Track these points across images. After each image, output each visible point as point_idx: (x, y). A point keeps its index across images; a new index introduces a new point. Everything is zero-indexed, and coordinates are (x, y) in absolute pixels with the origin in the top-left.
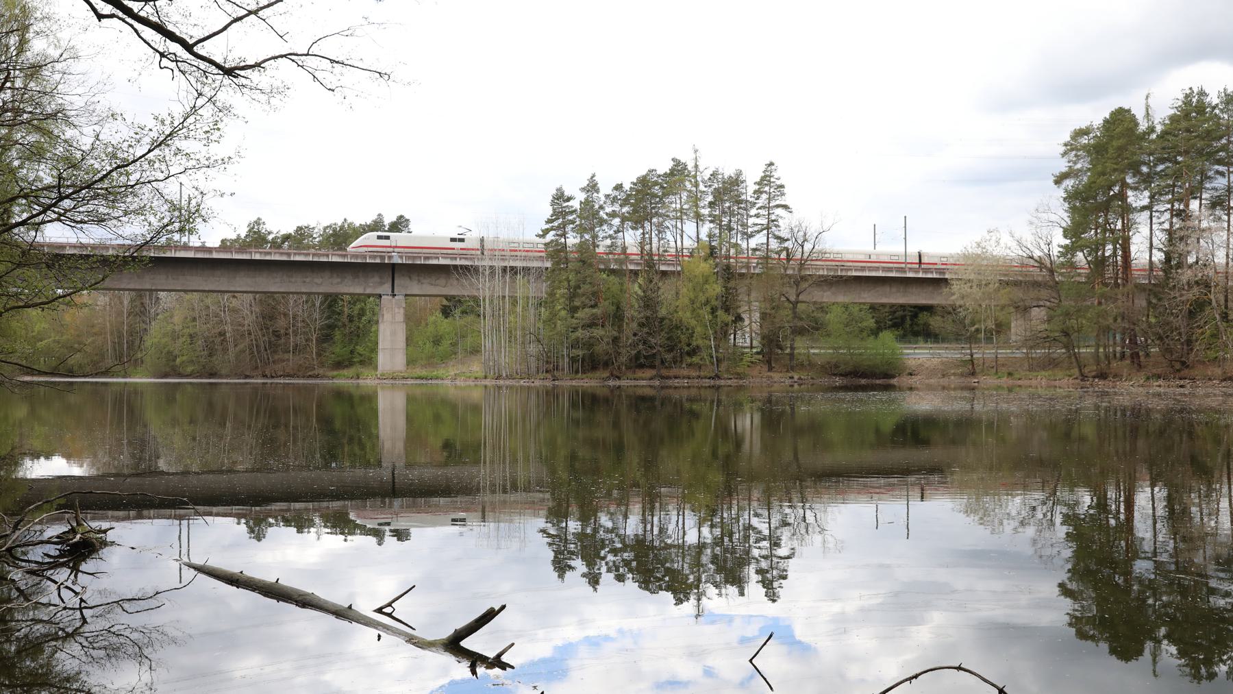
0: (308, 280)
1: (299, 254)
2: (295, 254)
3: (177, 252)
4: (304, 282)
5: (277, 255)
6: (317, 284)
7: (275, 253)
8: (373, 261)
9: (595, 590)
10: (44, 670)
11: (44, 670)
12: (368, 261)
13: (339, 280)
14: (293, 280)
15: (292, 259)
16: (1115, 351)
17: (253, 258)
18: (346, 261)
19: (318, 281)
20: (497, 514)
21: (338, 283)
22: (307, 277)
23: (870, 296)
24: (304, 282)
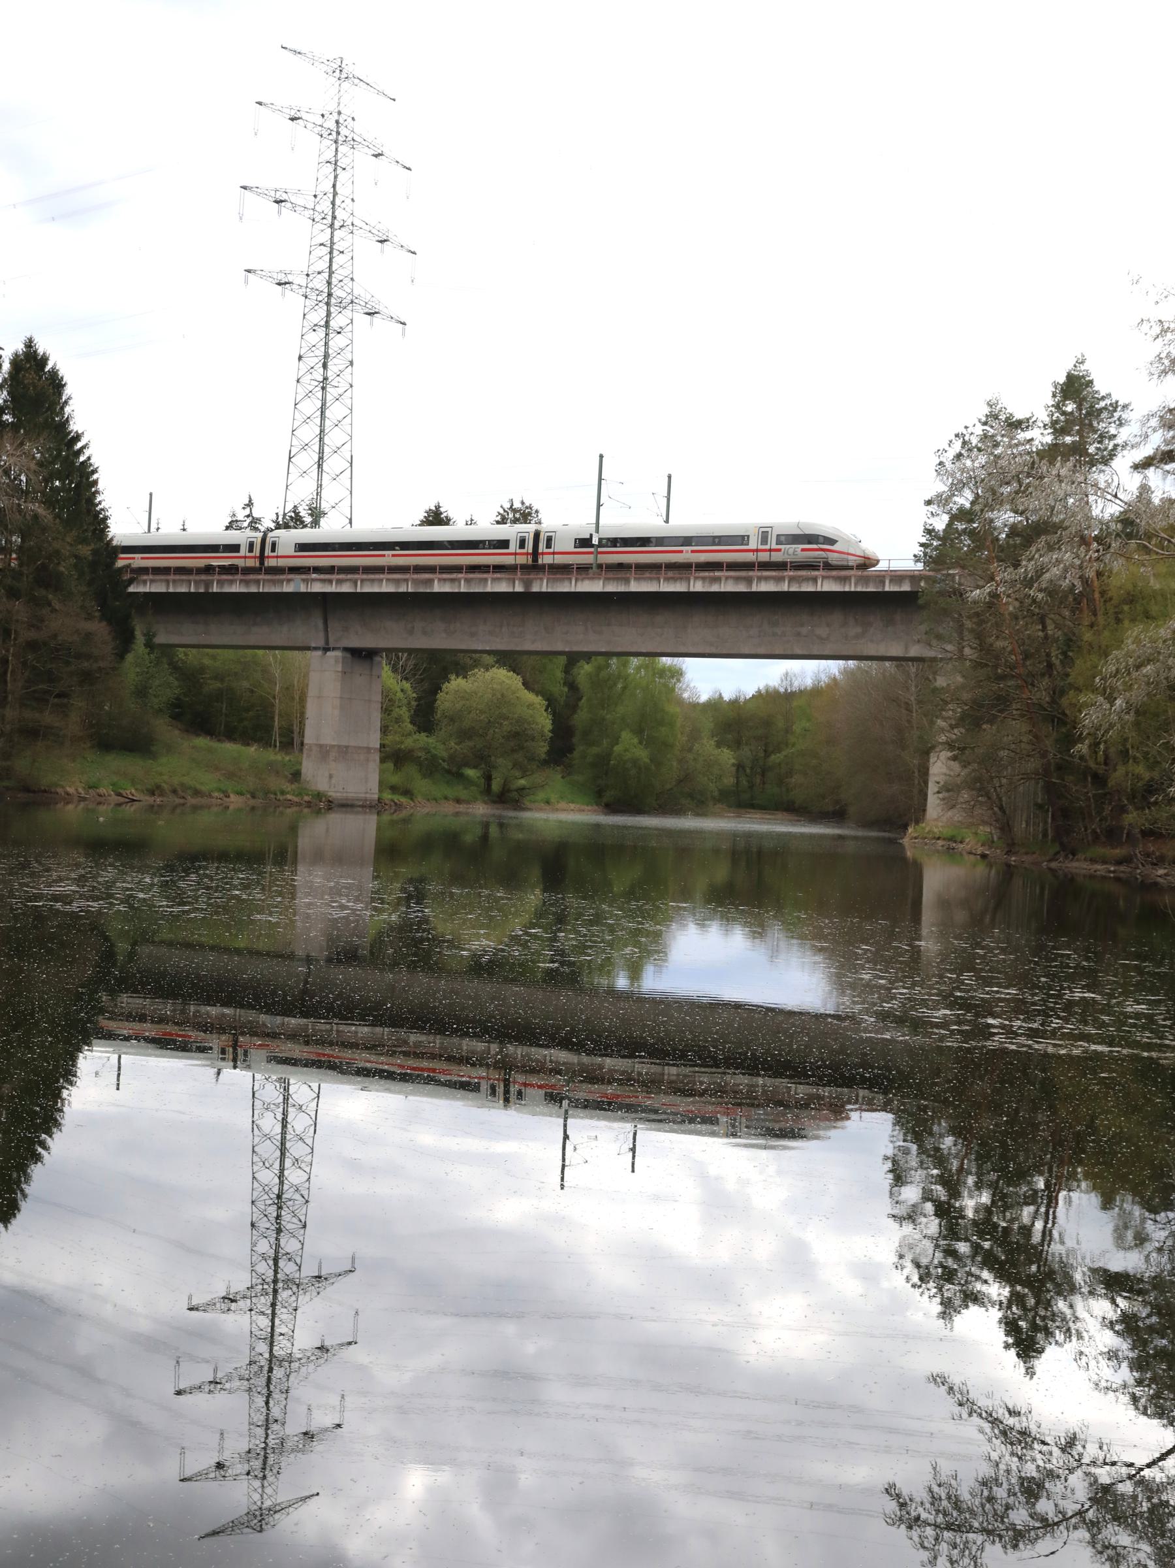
0: (804, 630)
1: (766, 579)
2: (760, 579)
3: (579, 583)
4: (799, 634)
5: (730, 582)
6: (820, 638)
7: (727, 578)
8: (896, 589)
9: (1030, 1372)
10: (1009, 771)
11: (1009, 771)
12: (887, 589)
13: (859, 630)
14: (778, 630)
15: (754, 589)
16: (1127, 665)
17: (692, 589)
18: (847, 589)
19: (822, 631)
20: (1163, 676)
21: (857, 637)
22: (802, 625)
23: (296, 729)
24: (799, 634)
